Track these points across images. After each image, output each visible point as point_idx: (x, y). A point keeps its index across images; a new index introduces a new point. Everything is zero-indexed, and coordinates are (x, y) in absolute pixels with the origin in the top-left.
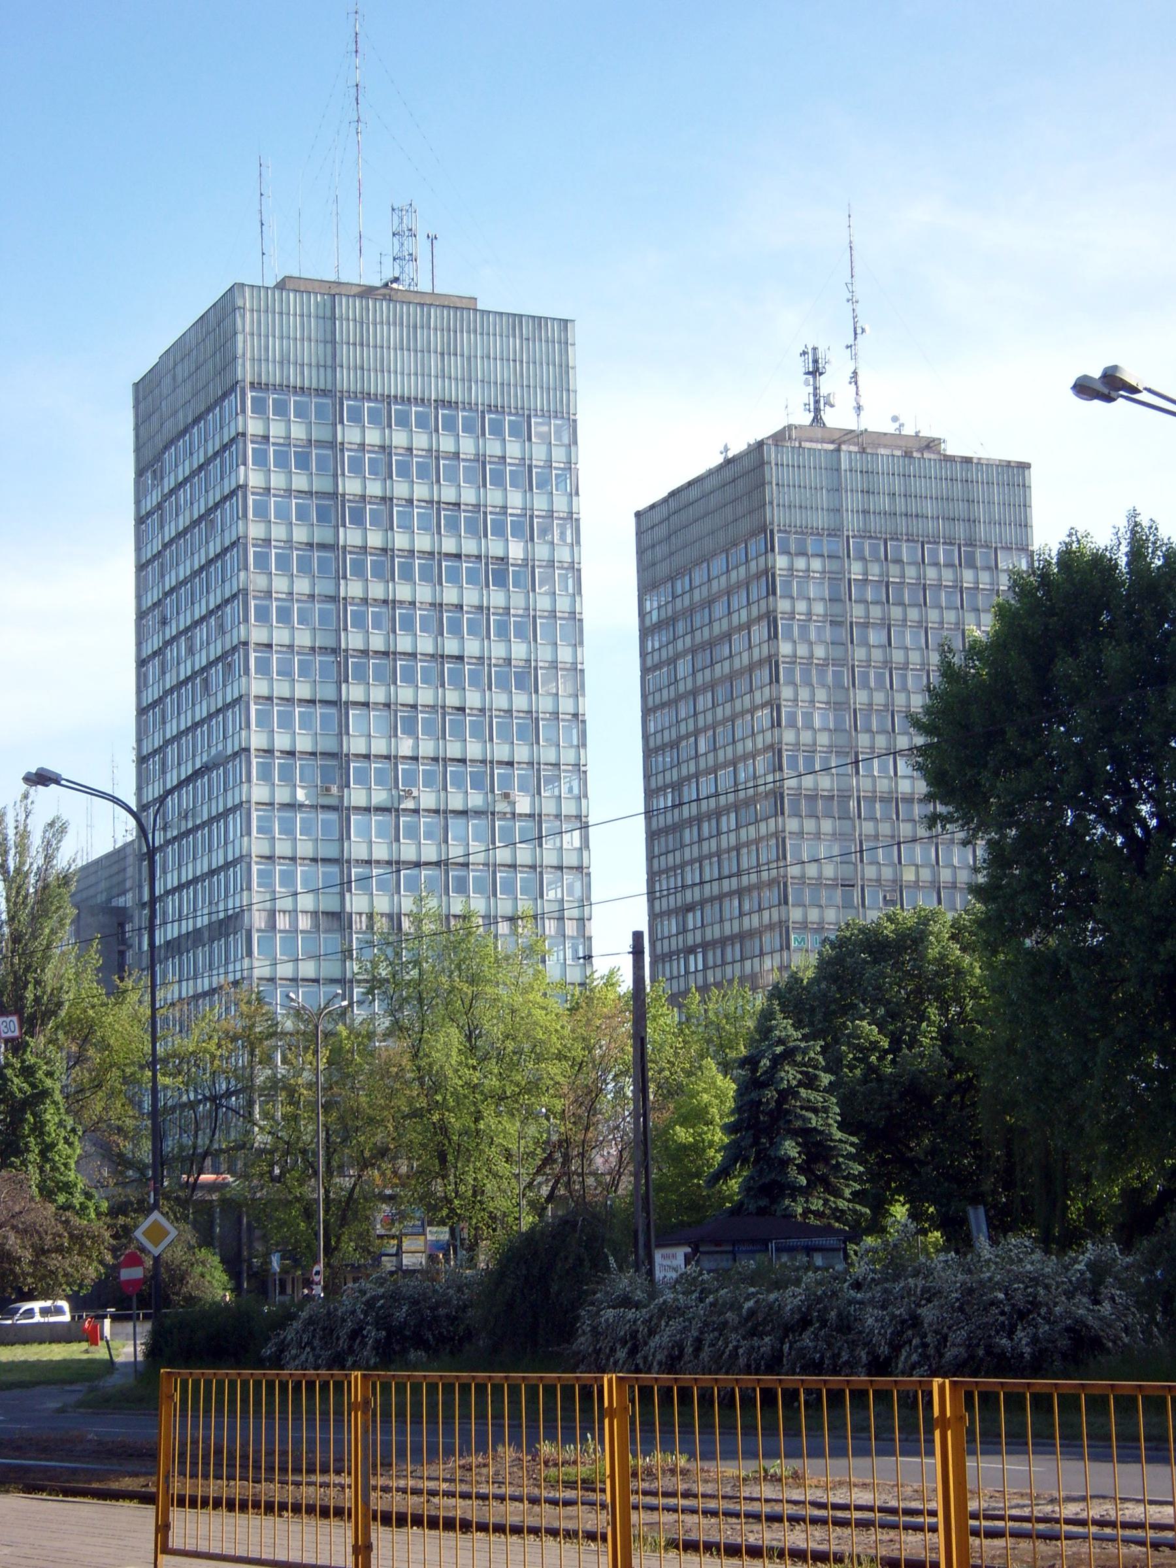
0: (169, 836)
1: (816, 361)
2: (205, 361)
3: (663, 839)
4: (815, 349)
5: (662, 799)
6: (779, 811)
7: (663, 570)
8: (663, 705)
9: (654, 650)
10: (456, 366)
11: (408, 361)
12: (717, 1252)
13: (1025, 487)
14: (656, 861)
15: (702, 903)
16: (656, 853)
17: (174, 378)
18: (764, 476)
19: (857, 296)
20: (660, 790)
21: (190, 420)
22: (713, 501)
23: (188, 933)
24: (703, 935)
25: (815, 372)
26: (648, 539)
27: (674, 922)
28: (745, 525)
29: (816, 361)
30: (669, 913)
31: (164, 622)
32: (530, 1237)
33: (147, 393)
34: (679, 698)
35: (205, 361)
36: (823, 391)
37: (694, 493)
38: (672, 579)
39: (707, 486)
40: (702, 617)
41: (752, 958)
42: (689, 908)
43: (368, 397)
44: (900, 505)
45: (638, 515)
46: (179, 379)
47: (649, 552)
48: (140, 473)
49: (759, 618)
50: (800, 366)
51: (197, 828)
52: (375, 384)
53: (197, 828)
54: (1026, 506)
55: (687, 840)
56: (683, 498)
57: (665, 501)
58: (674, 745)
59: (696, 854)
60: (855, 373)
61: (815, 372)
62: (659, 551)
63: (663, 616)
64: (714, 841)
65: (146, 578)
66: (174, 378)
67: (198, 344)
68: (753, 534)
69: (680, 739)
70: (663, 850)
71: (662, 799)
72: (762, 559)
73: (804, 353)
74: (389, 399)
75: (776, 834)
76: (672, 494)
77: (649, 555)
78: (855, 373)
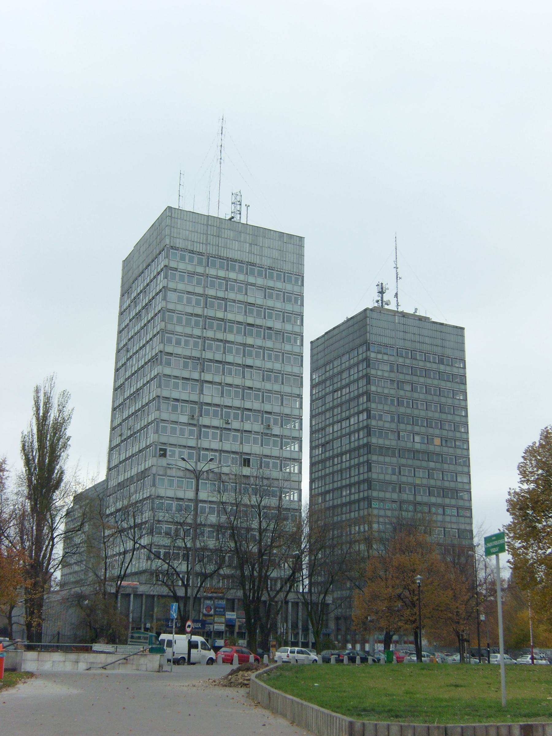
0: (123, 439)
1: (382, 288)
2: (153, 242)
3: (317, 466)
4: (382, 284)
5: (317, 450)
6: (369, 452)
7: (321, 362)
8: (319, 414)
9: (316, 393)
10: (256, 249)
11: (236, 245)
12: (141, 611)
13: (463, 336)
14: (313, 475)
15: (333, 490)
16: (314, 471)
17: (139, 253)
18: (366, 322)
19: (398, 266)
20: (317, 447)
21: (144, 267)
22: (344, 334)
23: (128, 479)
24: (333, 503)
25: (382, 292)
26: (315, 351)
27: (320, 498)
28: (357, 342)
29: (382, 288)
30: (318, 495)
31: (128, 351)
32: (246, 621)
33: (127, 263)
34: (327, 410)
35: (153, 242)
36: (385, 299)
37: (335, 332)
38: (325, 365)
39: (342, 328)
40: (338, 379)
41: (354, 512)
42: (328, 492)
43: (220, 258)
44: (417, 338)
45: (312, 342)
46: (142, 252)
47: (316, 356)
48: (122, 295)
49: (363, 377)
50: (376, 290)
51: (135, 433)
52: (224, 253)
53: (135, 433)
54: (463, 343)
55: (328, 466)
56: (331, 334)
57: (323, 336)
58: (323, 429)
59: (331, 471)
60: (397, 294)
61: (382, 292)
62: (320, 355)
63: (320, 380)
64: (339, 466)
65: (121, 337)
66: (139, 253)
67: (150, 236)
68: (361, 345)
69: (326, 426)
70: (317, 470)
71: (317, 450)
72: (364, 354)
73: (378, 285)
74: (228, 259)
75: (367, 461)
76: (326, 333)
77: (315, 357)
78: (397, 294)
